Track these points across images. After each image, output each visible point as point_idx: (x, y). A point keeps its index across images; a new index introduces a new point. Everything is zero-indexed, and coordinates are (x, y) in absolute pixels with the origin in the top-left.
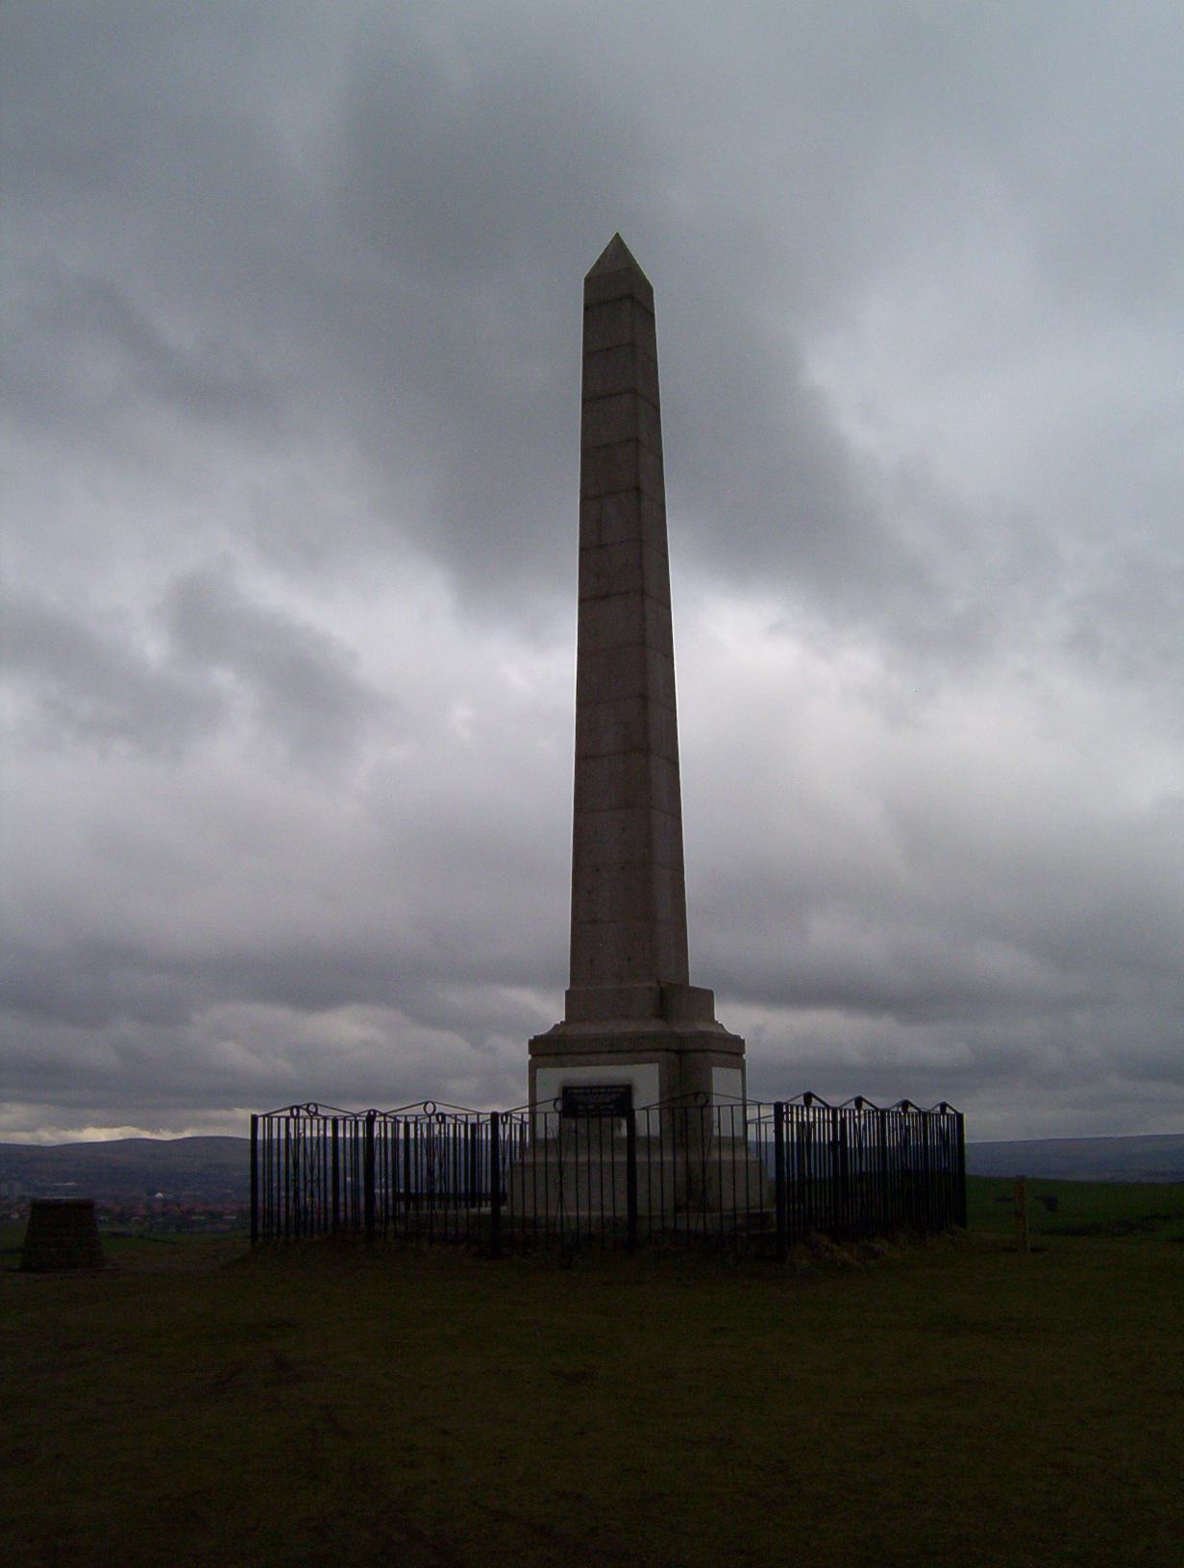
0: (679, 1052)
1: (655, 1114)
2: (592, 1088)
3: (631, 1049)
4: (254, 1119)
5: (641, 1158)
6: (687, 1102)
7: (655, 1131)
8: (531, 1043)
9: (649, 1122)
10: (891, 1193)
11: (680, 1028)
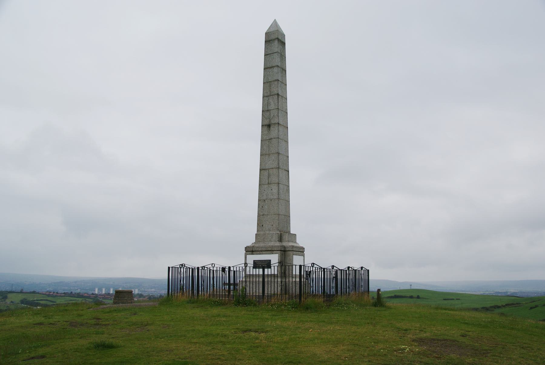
0: (285, 251)
1: (276, 268)
2: (531, 298)
3: (271, 251)
4: (169, 268)
5: (266, 280)
6: (284, 265)
7: (276, 273)
8: (246, 248)
9: (274, 270)
10: (346, 291)
11: (285, 244)
